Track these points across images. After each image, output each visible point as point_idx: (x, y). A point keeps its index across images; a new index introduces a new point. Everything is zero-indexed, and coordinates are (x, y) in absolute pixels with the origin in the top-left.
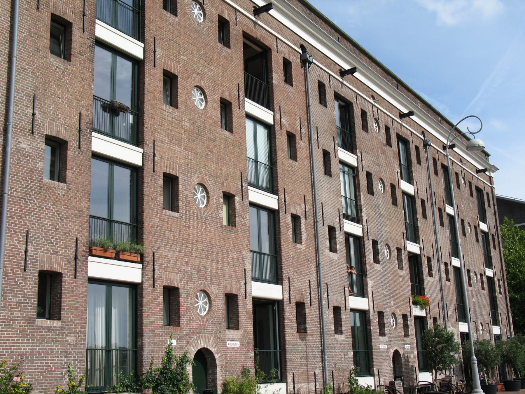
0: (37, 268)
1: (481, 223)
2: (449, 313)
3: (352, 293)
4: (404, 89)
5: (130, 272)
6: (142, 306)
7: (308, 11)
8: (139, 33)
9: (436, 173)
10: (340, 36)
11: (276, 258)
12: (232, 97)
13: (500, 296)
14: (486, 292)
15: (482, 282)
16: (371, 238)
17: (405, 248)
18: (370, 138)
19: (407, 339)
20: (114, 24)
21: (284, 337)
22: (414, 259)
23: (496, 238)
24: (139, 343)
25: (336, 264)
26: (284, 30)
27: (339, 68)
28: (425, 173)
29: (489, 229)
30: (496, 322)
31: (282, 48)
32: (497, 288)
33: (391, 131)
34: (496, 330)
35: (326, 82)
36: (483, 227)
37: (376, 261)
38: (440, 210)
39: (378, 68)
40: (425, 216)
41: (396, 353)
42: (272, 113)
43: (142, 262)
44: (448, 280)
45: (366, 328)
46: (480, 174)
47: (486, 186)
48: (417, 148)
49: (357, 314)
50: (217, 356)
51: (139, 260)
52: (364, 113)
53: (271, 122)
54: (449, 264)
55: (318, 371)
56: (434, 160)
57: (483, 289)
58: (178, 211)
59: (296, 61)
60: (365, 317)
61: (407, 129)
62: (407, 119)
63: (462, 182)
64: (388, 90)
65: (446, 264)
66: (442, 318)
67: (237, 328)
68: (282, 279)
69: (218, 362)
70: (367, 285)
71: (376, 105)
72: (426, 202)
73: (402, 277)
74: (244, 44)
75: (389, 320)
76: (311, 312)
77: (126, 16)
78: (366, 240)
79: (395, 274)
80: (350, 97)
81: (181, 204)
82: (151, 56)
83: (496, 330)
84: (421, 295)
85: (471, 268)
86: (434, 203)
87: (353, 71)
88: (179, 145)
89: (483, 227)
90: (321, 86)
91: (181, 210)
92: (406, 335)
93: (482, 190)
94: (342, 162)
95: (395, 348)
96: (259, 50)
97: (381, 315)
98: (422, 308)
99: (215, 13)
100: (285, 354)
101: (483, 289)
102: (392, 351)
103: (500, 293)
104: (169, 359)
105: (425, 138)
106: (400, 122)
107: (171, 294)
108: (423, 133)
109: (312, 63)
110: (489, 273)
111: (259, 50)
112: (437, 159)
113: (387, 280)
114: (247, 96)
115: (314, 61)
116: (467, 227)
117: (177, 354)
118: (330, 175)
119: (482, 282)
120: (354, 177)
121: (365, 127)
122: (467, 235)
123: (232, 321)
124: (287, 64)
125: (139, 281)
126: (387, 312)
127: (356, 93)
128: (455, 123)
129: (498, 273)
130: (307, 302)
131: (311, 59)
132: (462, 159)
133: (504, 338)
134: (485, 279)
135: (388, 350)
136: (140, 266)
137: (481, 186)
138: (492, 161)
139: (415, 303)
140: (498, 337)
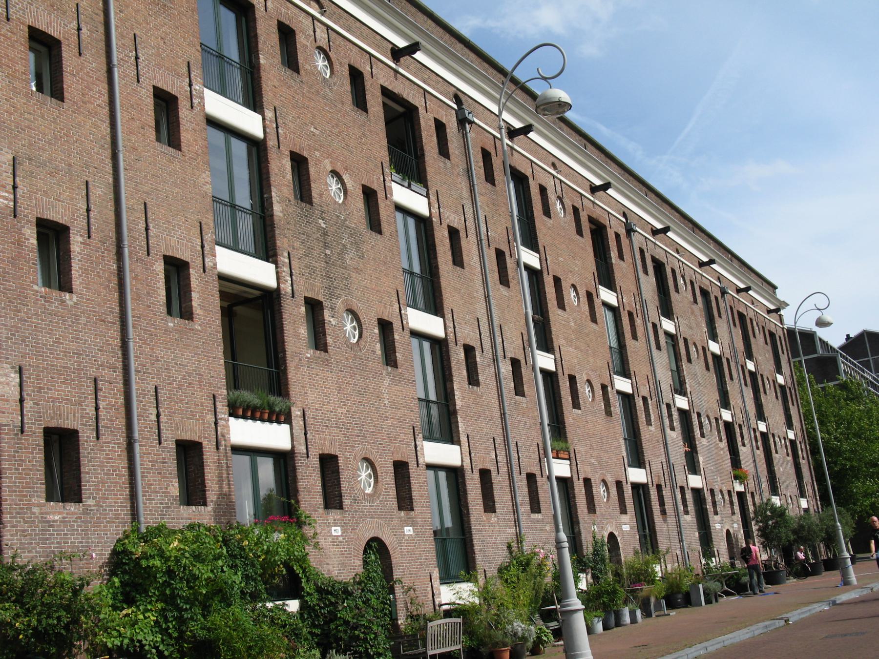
0: (41, 425)
1: (710, 342)
2: (763, 486)
3: (430, 438)
4: (653, 196)
5: (275, 436)
6: (574, 497)
7: (623, 172)
8: (253, 100)
9: (646, 272)
10: (586, 142)
11: (447, 406)
12: (175, 86)
13: (804, 462)
14: (790, 458)
15: (786, 447)
16: (566, 373)
17: (721, 417)
18: (555, 227)
19: (734, 517)
20: (223, 92)
21: (653, 520)
22: (728, 426)
23: (793, 391)
24: (576, 530)
25: (530, 414)
26: (435, 79)
27: (391, 46)
28: (725, 326)
29: (786, 381)
30: (802, 494)
31: (614, 222)
32: (800, 453)
33: (368, 82)
34: (804, 503)
35: (365, 69)
36: (714, 347)
37: (576, 405)
38: (654, 326)
39: (644, 188)
40: (731, 378)
41: (728, 531)
42: (538, 255)
43: (569, 459)
44: (758, 448)
45: (702, 508)
46: (597, 194)
47: (585, 201)
48: (617, 236)
49: (442, 475)
50: (619, 539)
51: (567, 457)
52: (673, 271)
53: (259, 133)
54: (672, 406)
55: (679, 552)
56: (642, 251)
57: (788, 455)
58: (580, 409)
59: (622, 232)
60: (700, 496)
61: (408, 83)
62: (601, 193)
63: (681, 282)
64: (553, 137)
65: (668, 406)
66: (504, 469)
67: (539, 512)
68: (644, 463)
69: (620, 545)
70: (699, 462)
71: (323, 19)
72: (635, 315)
73: (722, 449)
74: (384, 104)
75: (600, 491)
76: (499, 481)
77: (236, 78)
78: (636, 397)
79: (717, 447)
80: (526, 170)
81: (329, 340)
82: (544, 265)
83: (804, 503)
84: (280, 394)
85: (775, 432)
86: (484, 237)
87: (666, 230)
88: (571, 346)
89: (714, 347)
90: (642, 251)
91: (582, 407)
92: (733, 513)
93: (526, 178)
94: (399, 208)
95: (610, 530)
96: (401, 109)
97: (712, 491)
98: (741, 483)
99: (570, 204)
100: (656, 536)
101: (788, 455)
102: (725, 531)
103: (803, 458)
104: (596, 542)
105: (626, 219)
106: (592, 199)
107: (329, 465)
108: (719, 279)
109: (474, 122)
110: (791, 435)
111: (401, 109)
112: (645, 250)
113: (595, 433)
114: (600, 284)
115: (476, 120)
116: (692, 349)
117: (598, 537)
118: (58, 93)
119: (786, 447)
120: (673, 346)
121: (547, 212)
122: (768, 392)
123: (405, 501)
124: (440, 126)
125: (569, 475)
126: (596, 480)
127: (666, 251)
128: (508, 67)
129: (799, 434)
130: (663, 484)
131: (470, 117)
132: (556, 162)
133: (812, 511)
134: (758, 434)
135: (721, 530)
136: (568, 462)
137: (661, 257)
138: (780, 294)
139: (736, 478)
140: (806, 510)
